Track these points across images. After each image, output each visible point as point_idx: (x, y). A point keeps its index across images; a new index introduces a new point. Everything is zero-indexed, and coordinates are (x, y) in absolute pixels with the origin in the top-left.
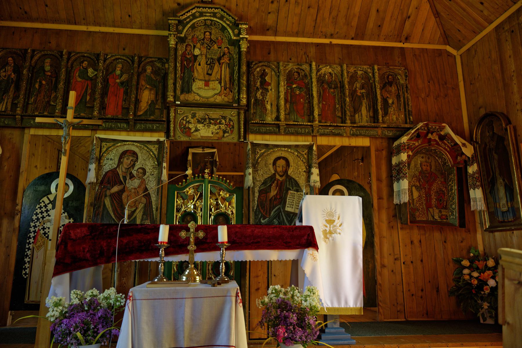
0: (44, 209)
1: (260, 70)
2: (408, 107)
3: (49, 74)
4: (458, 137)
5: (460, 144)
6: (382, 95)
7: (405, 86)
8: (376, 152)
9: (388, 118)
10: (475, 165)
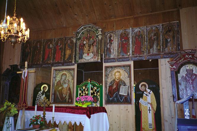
0: (39, 96)
1: (109, 35)
2: (178, 42)
3: (39, 48)
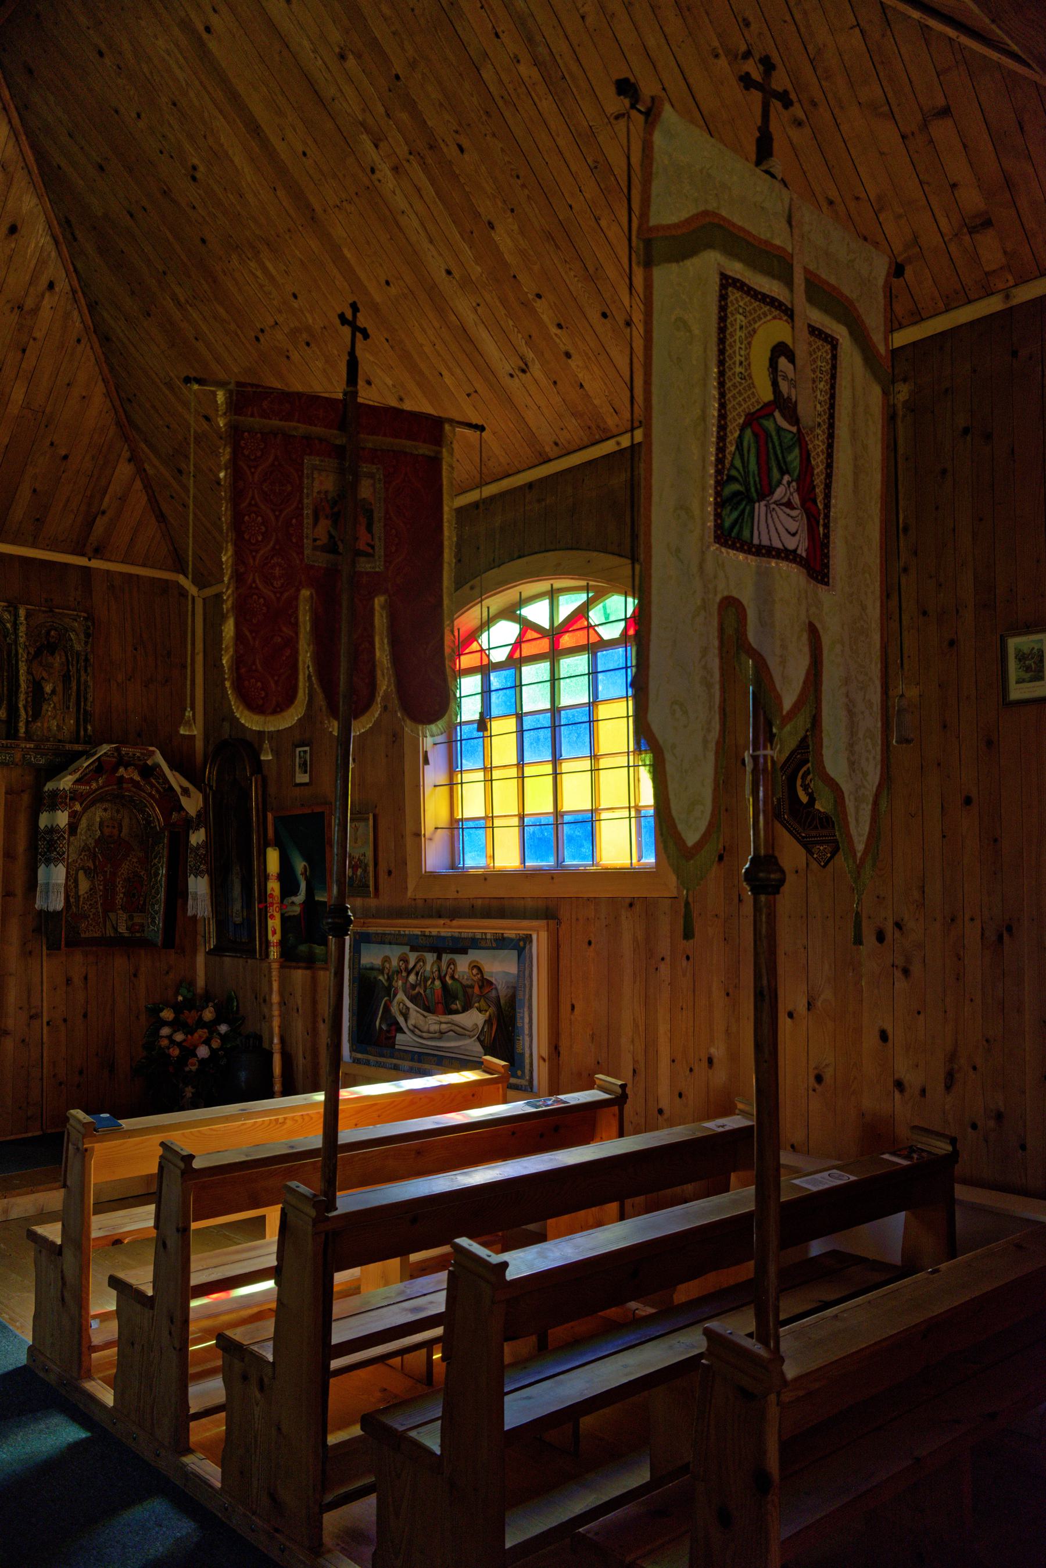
2: (85, 705)
4: (177, 774)
5: (178, 790)
6: (29, 672)
7: (83, 658)
8: (9, 796)
9: (39, 724)
10: (202, 830)
